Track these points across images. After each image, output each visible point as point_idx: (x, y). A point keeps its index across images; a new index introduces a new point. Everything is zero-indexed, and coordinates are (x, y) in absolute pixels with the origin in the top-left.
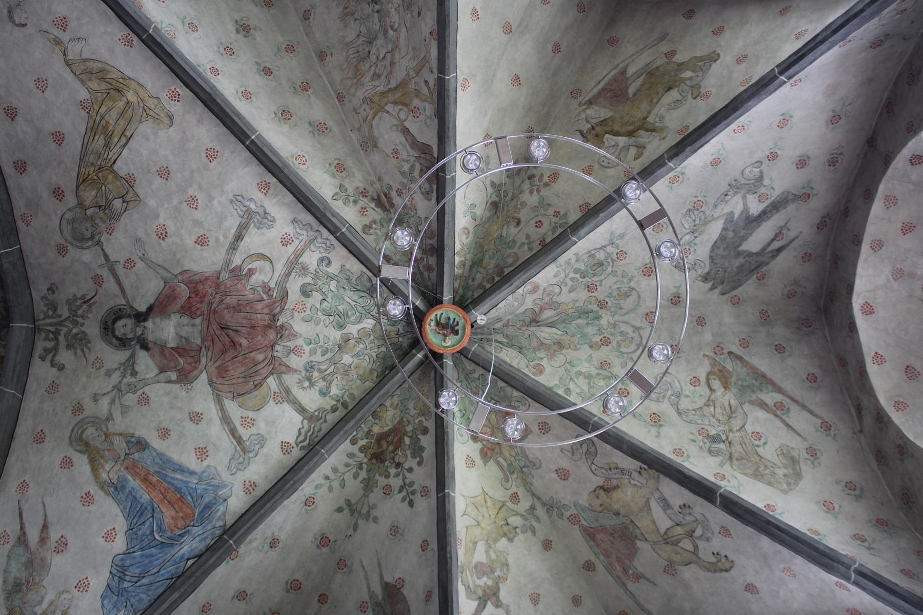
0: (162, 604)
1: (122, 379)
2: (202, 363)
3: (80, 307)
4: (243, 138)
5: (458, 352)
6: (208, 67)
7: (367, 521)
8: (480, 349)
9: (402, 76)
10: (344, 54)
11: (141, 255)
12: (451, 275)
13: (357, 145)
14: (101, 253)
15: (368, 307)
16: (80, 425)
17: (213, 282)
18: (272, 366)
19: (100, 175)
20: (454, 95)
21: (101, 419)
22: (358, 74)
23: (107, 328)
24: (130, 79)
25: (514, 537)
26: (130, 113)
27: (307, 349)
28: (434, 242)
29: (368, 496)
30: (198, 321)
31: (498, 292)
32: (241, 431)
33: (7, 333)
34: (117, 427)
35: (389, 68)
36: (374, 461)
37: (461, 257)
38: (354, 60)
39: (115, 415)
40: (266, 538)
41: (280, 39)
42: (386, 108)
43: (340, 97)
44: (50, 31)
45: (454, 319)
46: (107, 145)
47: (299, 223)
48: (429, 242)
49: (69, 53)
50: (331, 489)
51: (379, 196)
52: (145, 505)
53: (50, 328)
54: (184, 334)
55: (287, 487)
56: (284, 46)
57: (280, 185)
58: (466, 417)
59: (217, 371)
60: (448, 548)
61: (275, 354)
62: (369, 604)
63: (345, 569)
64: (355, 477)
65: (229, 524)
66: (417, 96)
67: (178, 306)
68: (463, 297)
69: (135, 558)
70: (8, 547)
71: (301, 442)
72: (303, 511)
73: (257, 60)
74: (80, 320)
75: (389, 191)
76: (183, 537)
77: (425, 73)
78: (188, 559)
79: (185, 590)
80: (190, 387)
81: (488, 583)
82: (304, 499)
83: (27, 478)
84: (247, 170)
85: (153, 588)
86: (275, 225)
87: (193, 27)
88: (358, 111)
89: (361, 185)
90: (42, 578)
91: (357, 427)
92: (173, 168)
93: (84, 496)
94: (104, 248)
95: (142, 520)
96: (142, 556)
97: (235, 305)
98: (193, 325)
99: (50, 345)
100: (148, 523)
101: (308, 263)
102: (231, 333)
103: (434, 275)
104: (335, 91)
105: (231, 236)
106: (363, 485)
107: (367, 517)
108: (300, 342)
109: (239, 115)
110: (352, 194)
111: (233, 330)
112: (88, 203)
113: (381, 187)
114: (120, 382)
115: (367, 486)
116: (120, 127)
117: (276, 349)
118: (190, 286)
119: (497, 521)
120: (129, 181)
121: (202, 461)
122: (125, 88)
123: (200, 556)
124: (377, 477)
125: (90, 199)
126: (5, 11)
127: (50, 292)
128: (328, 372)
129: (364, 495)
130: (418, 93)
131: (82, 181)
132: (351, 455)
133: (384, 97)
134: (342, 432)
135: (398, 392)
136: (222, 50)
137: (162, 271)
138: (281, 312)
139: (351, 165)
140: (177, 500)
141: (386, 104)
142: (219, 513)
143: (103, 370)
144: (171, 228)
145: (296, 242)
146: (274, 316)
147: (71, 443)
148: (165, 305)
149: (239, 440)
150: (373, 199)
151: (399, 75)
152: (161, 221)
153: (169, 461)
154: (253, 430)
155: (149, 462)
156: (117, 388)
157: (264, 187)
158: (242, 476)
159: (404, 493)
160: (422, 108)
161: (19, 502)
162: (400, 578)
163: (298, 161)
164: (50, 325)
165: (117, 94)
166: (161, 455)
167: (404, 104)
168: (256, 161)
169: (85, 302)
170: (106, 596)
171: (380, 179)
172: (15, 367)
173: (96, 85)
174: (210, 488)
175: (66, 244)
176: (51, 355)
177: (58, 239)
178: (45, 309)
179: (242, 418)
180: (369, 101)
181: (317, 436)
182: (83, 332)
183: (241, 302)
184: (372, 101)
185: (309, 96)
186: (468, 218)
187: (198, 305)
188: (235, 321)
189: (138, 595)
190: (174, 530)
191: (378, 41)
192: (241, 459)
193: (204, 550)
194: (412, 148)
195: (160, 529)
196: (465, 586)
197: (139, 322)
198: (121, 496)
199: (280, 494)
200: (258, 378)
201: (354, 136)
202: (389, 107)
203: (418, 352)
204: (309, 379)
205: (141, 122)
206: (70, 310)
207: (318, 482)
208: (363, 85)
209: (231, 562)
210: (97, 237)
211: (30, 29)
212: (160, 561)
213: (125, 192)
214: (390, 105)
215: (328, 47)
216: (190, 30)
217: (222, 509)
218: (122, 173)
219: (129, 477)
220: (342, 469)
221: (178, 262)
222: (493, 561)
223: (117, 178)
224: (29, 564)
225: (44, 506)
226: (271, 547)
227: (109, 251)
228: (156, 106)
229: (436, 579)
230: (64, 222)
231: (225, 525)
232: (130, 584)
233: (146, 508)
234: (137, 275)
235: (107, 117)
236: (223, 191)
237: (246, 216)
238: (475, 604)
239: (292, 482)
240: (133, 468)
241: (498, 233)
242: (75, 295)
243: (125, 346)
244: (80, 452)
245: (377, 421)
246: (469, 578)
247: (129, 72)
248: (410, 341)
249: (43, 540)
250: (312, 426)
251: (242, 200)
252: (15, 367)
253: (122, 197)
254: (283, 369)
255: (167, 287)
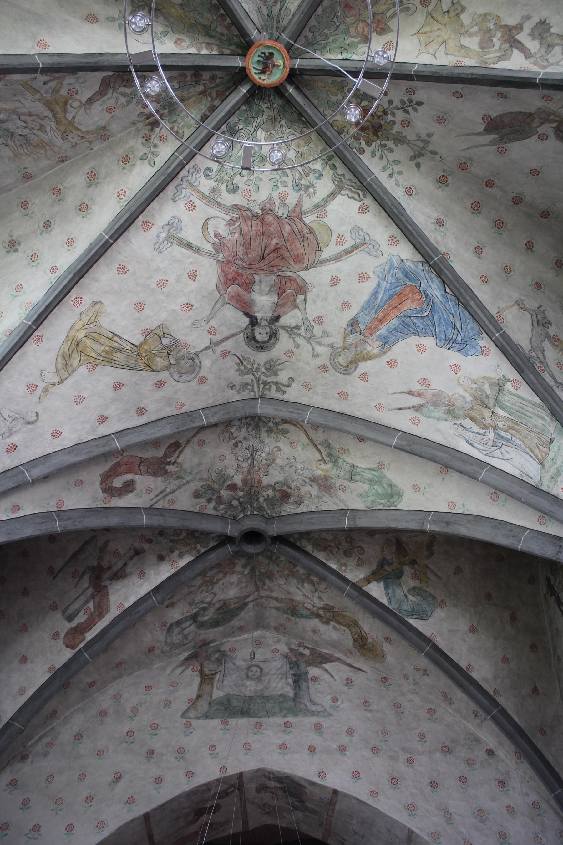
0: (476, 313)
1: (302, 336)
2: (291, 275)
3: (245, 367)
4: (109, 244)
5: (288, 52)
6: (50, 275)
7: (430, 142)
8: (287, 31)
9: (41, 105)
10: (24, 157)
11: (205, 323)
12: (219, 59)
13: (104, 144)
14: (204, 352)
15: (247, 135)
16: (336, 367)
17: (226, 266)
18: (295, 219)
19: (144, 355)
20: (56, 57)
21: (332, 352)
22: (41, 145)
23: (262, 347)
24: (67, 336)
25: (461, 5)
26: (94, 335)
27: (282, 189)
28: (189, 74)
29: (409, 141)
30: (257, 278)
31: (235, 12)
32: (348, 245)
33: (265, 417)
34: (339, 341)
35: (34, 117)
36: (380, 134)
37: (202, 47)
38: (29, 148)
39: (330, 342)
40: (436, 229)
41: (17, 214)
42: (70, 119)
43: (63, 160)
44: (38, 396)
45: (259, 56)
46: (121, 351)
47: (175, 195)
48: (189, 78)
49: (53, 381)
50: (400, 173)
51: (149, 124)
52: (401, 322)
53: (261, 388)
54: (267, 289)
55: (396, 212)
56: (23, 211)
57: (145, 212)
58: (347, 47)
59: (298, 264)
60: (463, 76)
61: (285, 216)
62: (500, 146)
63: (468, 164)
64: (392, 151)
65: (421, 259)
66: (58, 91)
67: (245, 293)
68: (239, 46)
69: (440, 332)
70: (421, 417)
71: (360, 197)
72: (416, 197)
73: (38, 234)
74: (255, 366)
75: (144, 115)
76: (428, 295)
77: (36, 84)
78: (446, 292)
79: (469, 296)
80: (310, 285)
81: (499, 37)
82: (407, 196)
83: (373, 405)
84: (133, 240)
85: (464, 319)
86: (178, 216)
87: (19, 288)
88: (74, 144)
89: (140, 140)
90: (447, 396)
91: (349, 148)
92: (136, 300)
93: (390, 365)
94: (200, 350)
95: (412, 324)
96: (439, 326)
97: (244, 248)
98: (260, 281)
99: (274, 388)
100: (415, 321)
101: (209, 187)
102: (267, 252)
103: (218, 74)
104: (57, 164)
105: (188, 252)
106: (399, 145)
107: (426, 142)
108: (275, 195)
109: (89, 250)
110: (149, 149)
111: (265, 250)
112: (166, 363)
113: (140, 122)
114: (304, 338)
115: (400, 141)
116: (106, 342)
117: (282, 215)
118: (229, 284)
119: (444, 23)
120: (148, 333)
121: (369, 278)
122: (75, 339)
123: (444, 282)
124: (393, 132)
125: (163, 362)
126: (29, 426)
127: (234, 388)
128: (302, 171)
129: (408, 144)
130: (55, 91)
131: (149, 368)
132: (373, 154)
133: (61, 121)
134: (354, 162)
135: (321, 110)
136: (34, 264)
137: (218, 306)
138: (250, 211)
139: (123, 149)
140: (399, 298)
141: (67, 119)
142: (412, 266)
143: (295, 350)
144: (184, 300)
145: (192, 198)
146: (253, 216)
147: (349, 374)
148: (244, 303)
149: (355, 248)
150: (152, 130)
151: (39, 108)
152: (178, 308)
153: (368, 303)
154: (347, 235)
155: (367, 318)
156: (309, 340)
157: (147, 226)
158: (384, 247)
159: (410, 109)
160: (69, 87)
161: (390, 410)
162: (483, 119)
163: (123, 197)
164: (259, 387)
165: (80, 345)
166: (363, 309)
167: (66, 103)
168: (125, 233)
169: (242, 363)
170: (466, 353)
171: (134, 123)
172: (290, 412)
173: (75, 361)
174: (391, 273)
175: (198, 378)
176: (282, 387)
177: (194, 383)
178: (247, 391)
179: (337, 245)
180: (65, 135)
181: (355, 183)
182: (264, 365)
183: (242, 243)
184: (65, 132)
185: (65, 188)
186: (166, 39)
187: (244, 277)
188: (257, 248)
189: (468, 330)
190: (422, 301)
191: (10, 127)
192: (371, 246)
193: (440, 279)
194: (105, 95)
195: (420, 311)
196: (498, 61)
197: (257, 323)
198: (392, 339)
199: (401, 217)
200: (305, 230)
201: (97, 147)
202: (70, 116)
203: (288, 91)
204: (307, 188)
205: (101, 326)
206: (247, 374)
207: (394, 183)
208: (51, 141)
209: (451, 259)
210: (192, 355)
211: (39, 409)
212: (444, 313)
213: (156, 336)
214: (67, 116)
215: (19, 172)
216: (22, 290)
217: (408, 264)
218: (142, 339)
219: (378, 333)
220: (384, 162)
221: (210, 294)
222: (480, 30)
223: (145, 342)
224: (436, 404)
225: (394, 393)
226: (443, 225)
227: (203, 347)
228: (87, 315)
229: (488, 88)
230: (181, 380)
231: (422, 262)
232: (459, 335)
233: (403, 321)
234: (221, 325)
235: (99, 352)
236: (152, 260)
237: (172, 240)
238: (516, 52)
239: (392, 207)
240: (371, 330)
241: (178, 9)
242: (237, 371)
243: (276, 334)
244: (356, 367)
245: (346, 130)
246: (492, 56)
247: (63, 337)
248: (277, 98)
249: (419, 395)
250: (346, 186)
251: (158, 244)
252: (290, 412)
253: (160, 338)
254: (297, 209)
255: (230, 302)
